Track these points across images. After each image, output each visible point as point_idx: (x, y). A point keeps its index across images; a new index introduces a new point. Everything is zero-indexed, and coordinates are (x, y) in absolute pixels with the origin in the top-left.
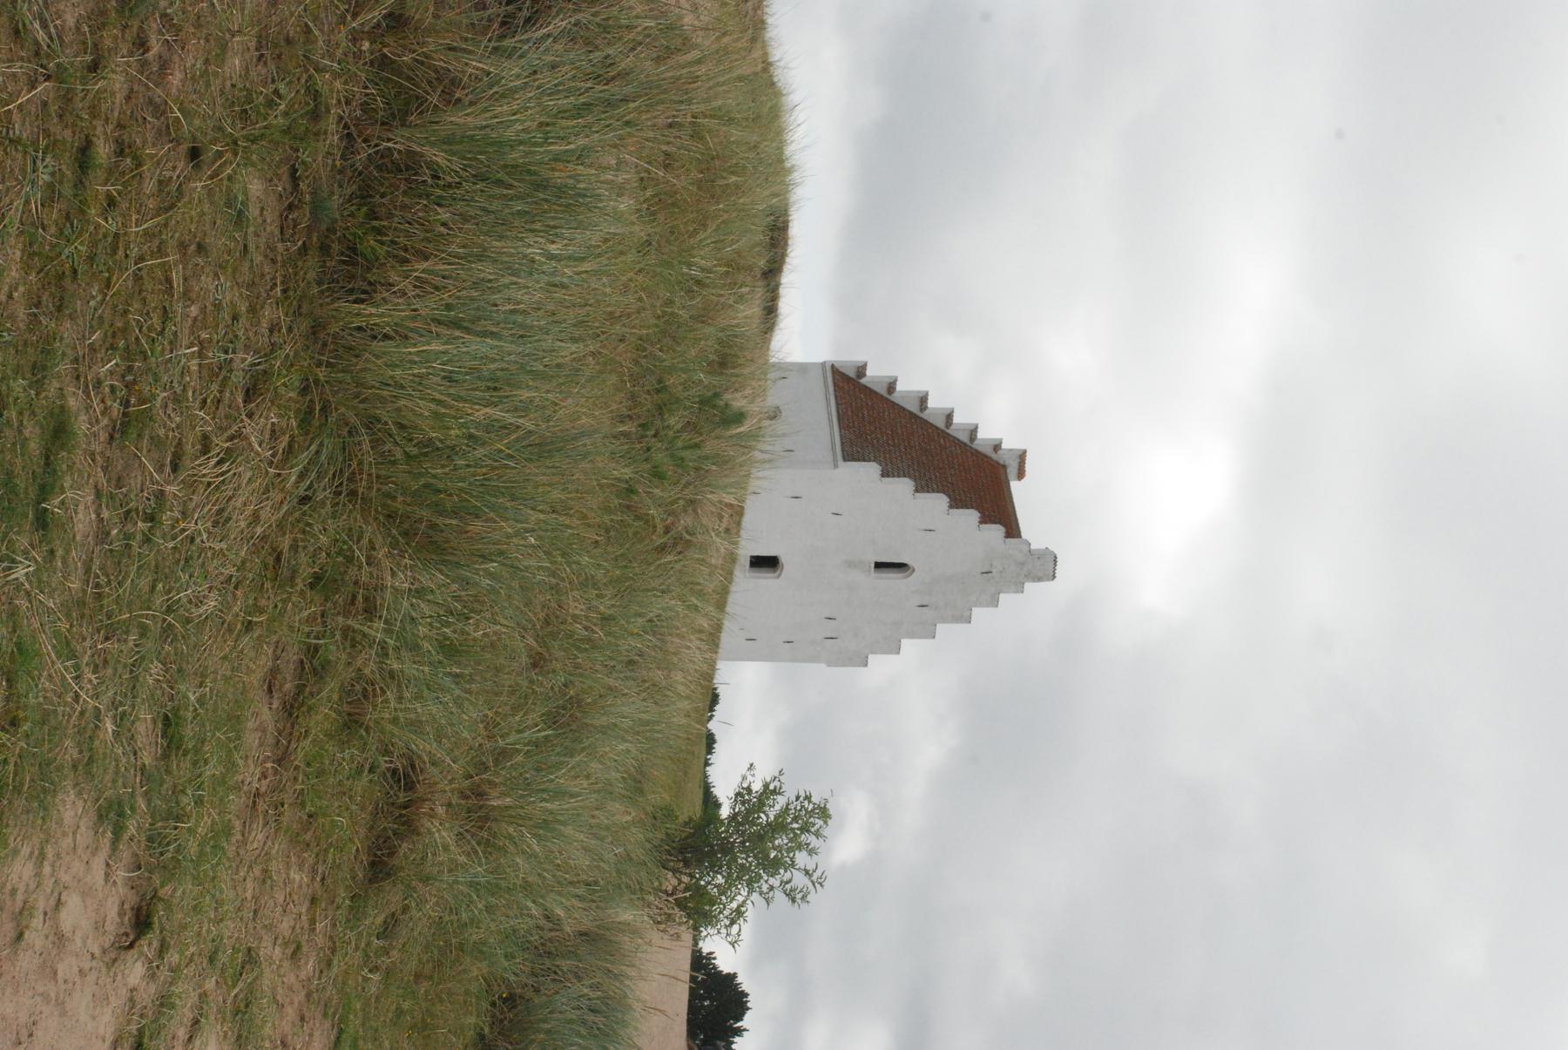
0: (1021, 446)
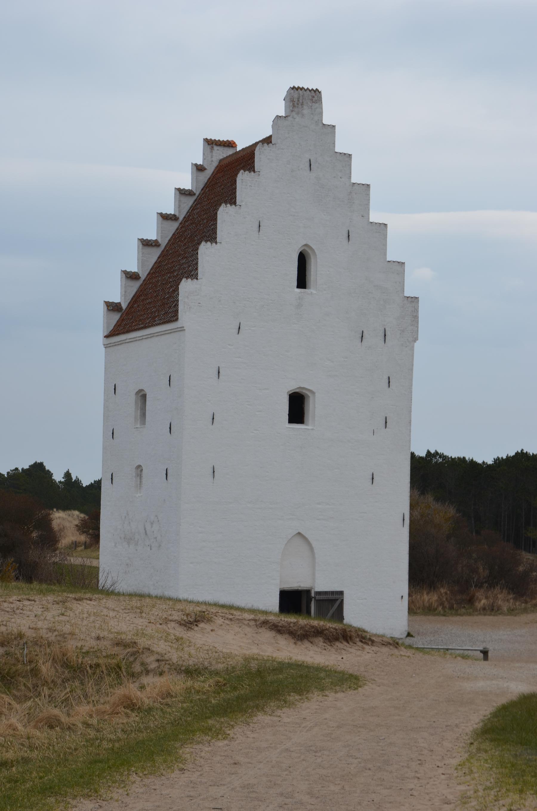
0: (201, 144)
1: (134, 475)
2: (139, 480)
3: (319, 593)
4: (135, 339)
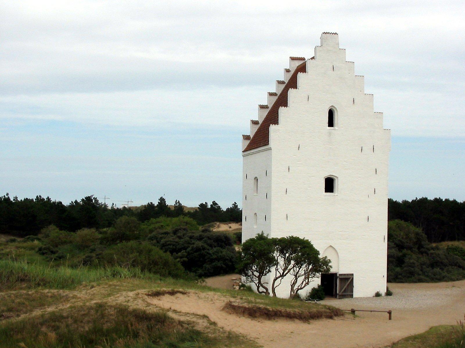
3: (341, 275)
4: (253, 153)
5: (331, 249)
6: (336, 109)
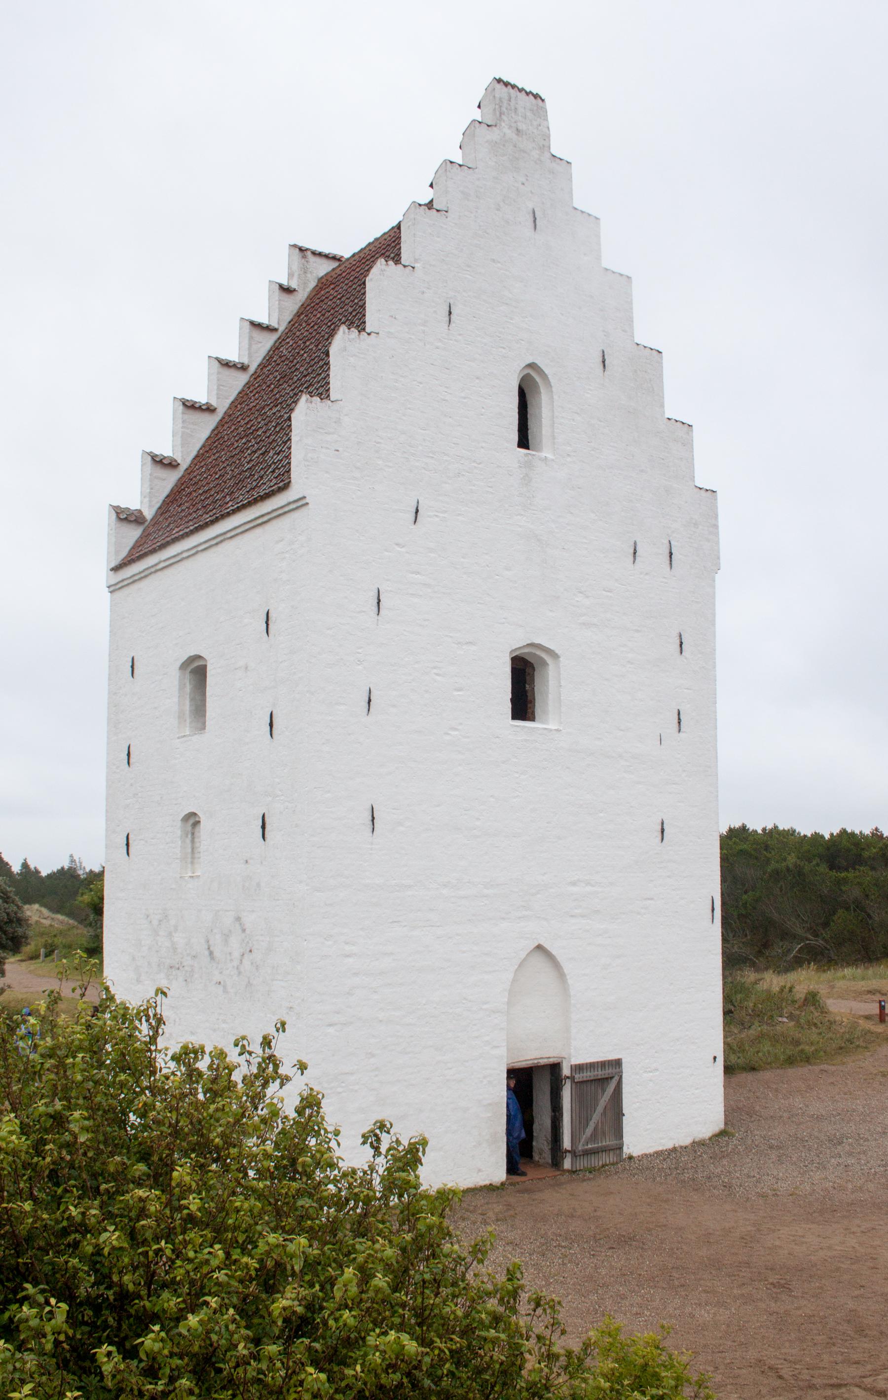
1: (179, 833)
2: (189, 845)
3: (579, 1068)
5: (539, 961)
6: (548, 384)
